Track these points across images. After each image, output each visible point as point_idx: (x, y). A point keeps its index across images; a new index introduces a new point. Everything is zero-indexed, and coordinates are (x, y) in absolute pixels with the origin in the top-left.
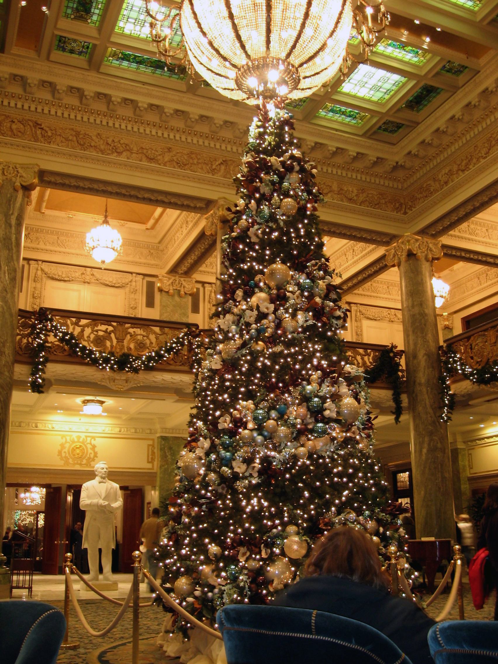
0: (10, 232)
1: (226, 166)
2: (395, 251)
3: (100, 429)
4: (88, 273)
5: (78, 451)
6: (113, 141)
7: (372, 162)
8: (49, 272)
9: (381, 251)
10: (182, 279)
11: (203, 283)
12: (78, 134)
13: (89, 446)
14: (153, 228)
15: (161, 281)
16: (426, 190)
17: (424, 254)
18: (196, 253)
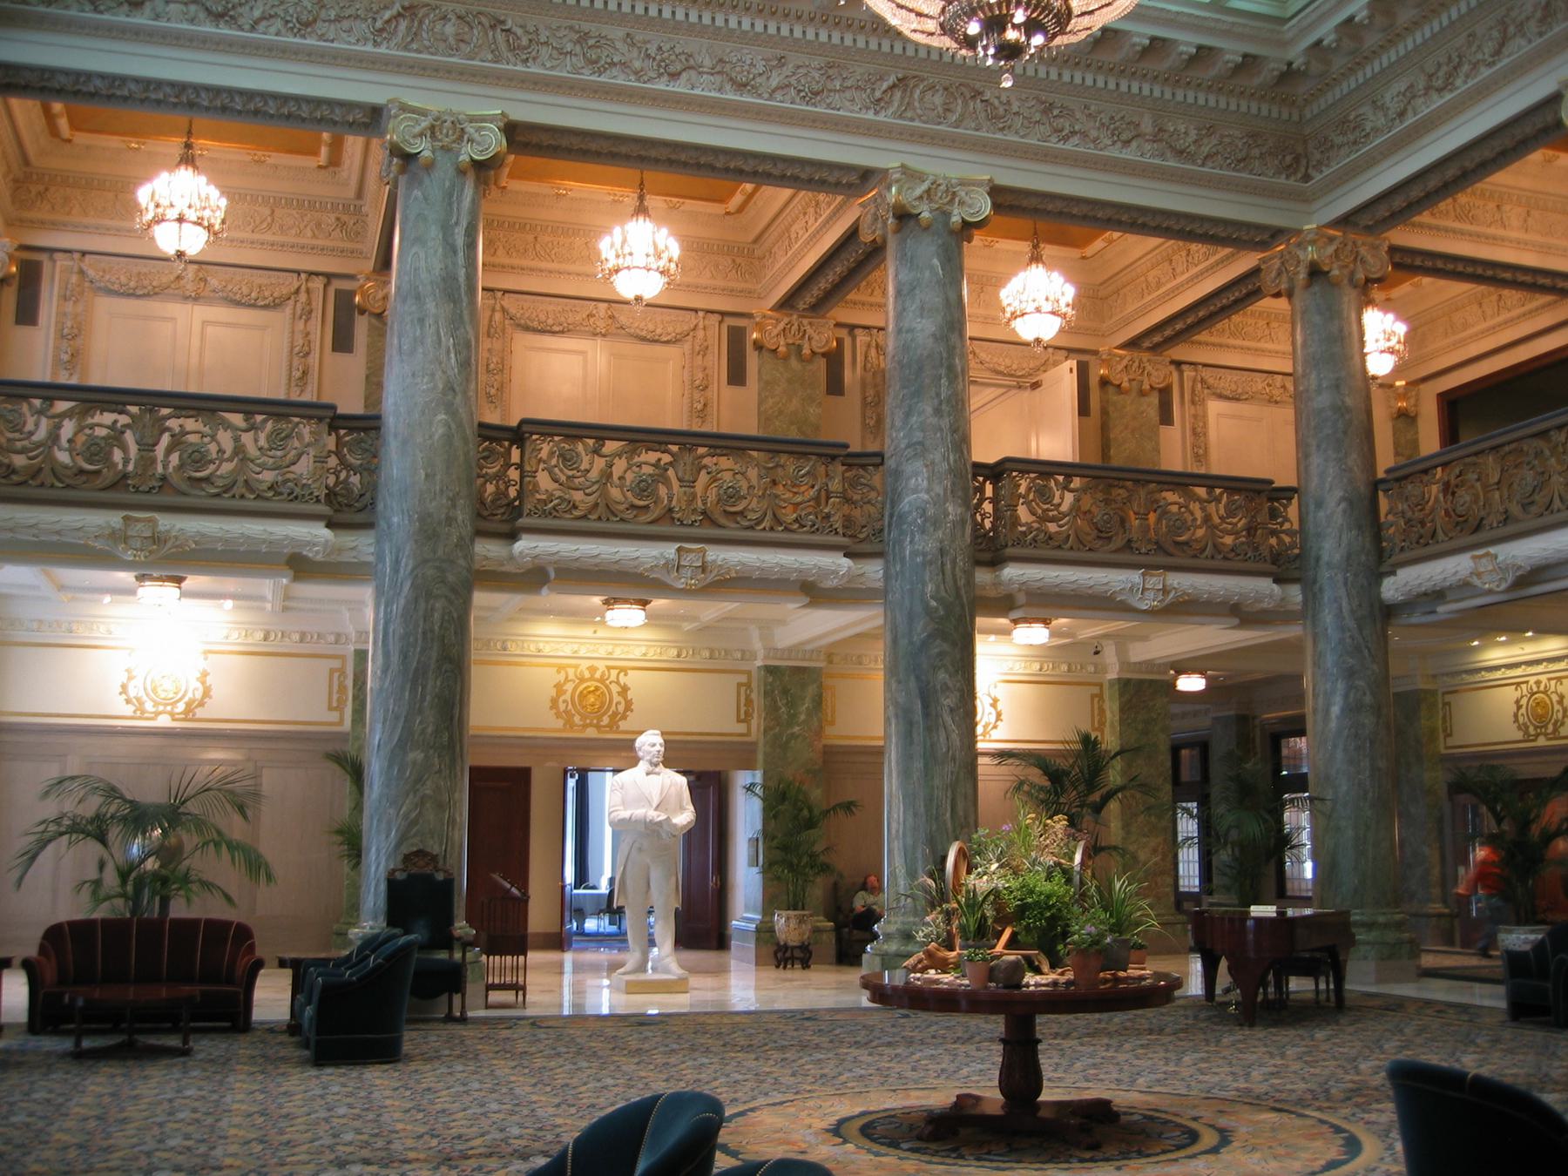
0: (454, 264)
1: (905, 91)
2: (1283, 263)
3: (637, 653)
4: (602, 314)
5: (592, 699)
6: (660, 48)
7: (1230, 65)
8: (518, 315)
9: (1246, 262)
10: (805, 321)
11: (852, 328)
12: (583, 38)
13: (615, 689)
14: (741, 209)
15: (760, 327)
16: (1354, 128)
17: (1346, 272)
18: (838, 270)
